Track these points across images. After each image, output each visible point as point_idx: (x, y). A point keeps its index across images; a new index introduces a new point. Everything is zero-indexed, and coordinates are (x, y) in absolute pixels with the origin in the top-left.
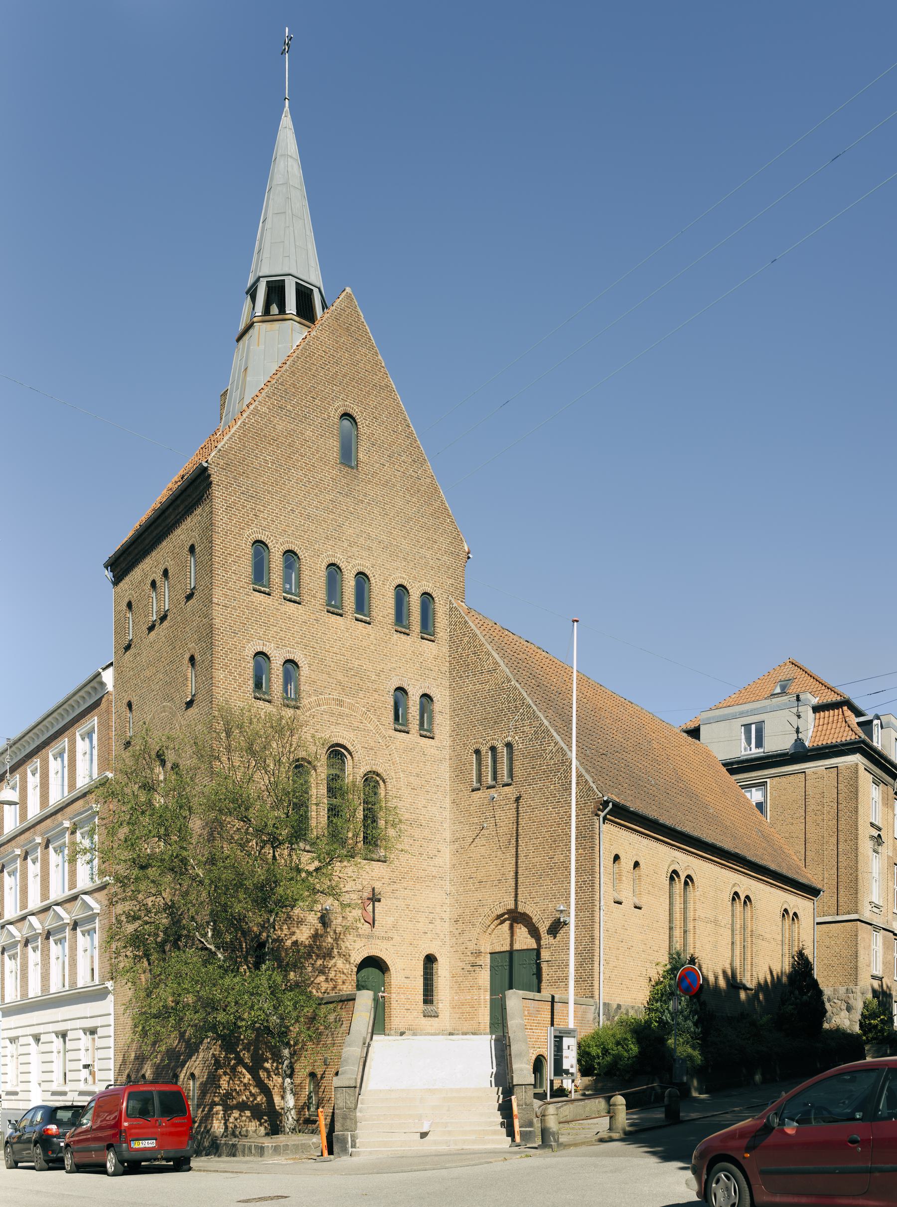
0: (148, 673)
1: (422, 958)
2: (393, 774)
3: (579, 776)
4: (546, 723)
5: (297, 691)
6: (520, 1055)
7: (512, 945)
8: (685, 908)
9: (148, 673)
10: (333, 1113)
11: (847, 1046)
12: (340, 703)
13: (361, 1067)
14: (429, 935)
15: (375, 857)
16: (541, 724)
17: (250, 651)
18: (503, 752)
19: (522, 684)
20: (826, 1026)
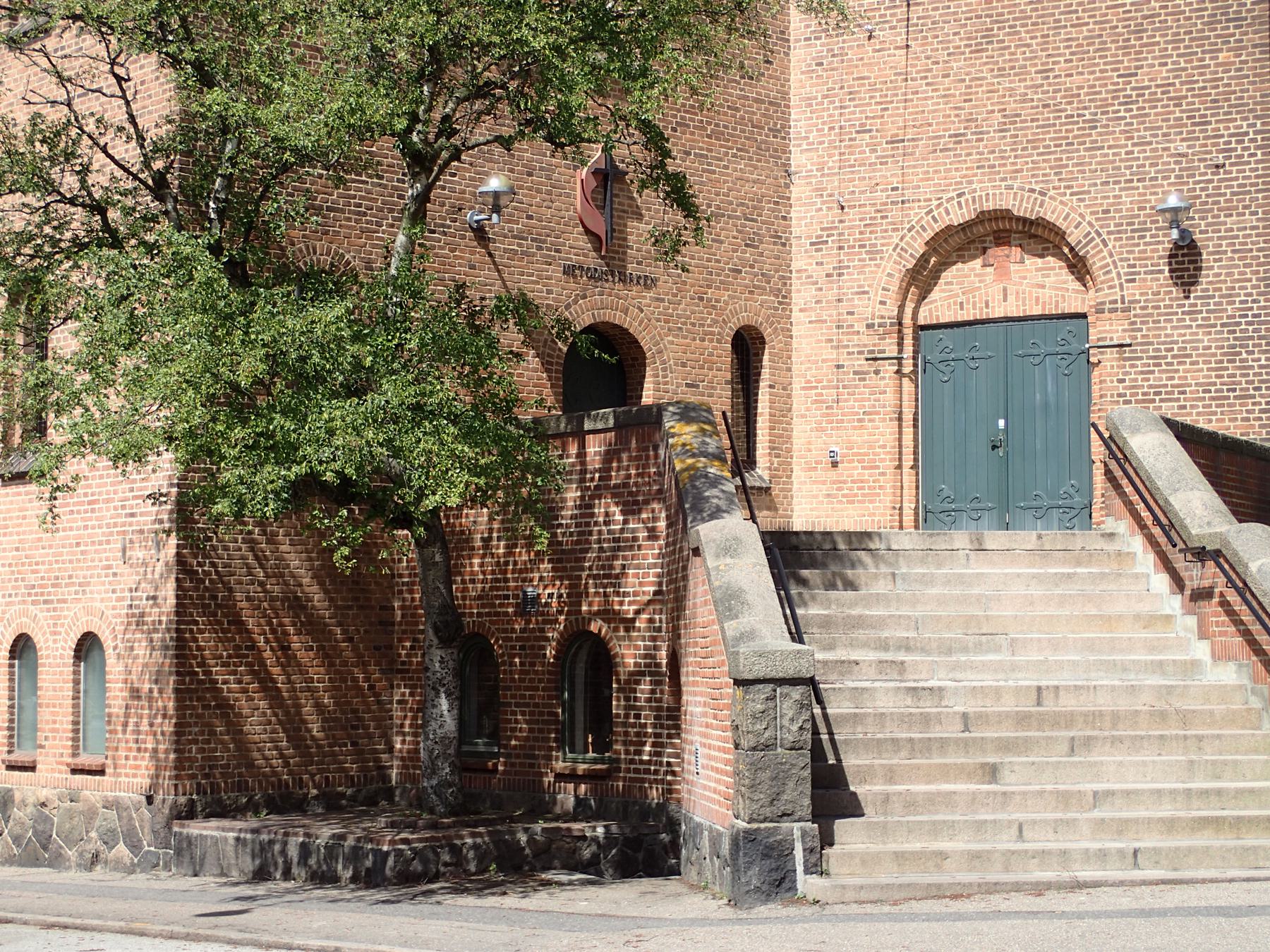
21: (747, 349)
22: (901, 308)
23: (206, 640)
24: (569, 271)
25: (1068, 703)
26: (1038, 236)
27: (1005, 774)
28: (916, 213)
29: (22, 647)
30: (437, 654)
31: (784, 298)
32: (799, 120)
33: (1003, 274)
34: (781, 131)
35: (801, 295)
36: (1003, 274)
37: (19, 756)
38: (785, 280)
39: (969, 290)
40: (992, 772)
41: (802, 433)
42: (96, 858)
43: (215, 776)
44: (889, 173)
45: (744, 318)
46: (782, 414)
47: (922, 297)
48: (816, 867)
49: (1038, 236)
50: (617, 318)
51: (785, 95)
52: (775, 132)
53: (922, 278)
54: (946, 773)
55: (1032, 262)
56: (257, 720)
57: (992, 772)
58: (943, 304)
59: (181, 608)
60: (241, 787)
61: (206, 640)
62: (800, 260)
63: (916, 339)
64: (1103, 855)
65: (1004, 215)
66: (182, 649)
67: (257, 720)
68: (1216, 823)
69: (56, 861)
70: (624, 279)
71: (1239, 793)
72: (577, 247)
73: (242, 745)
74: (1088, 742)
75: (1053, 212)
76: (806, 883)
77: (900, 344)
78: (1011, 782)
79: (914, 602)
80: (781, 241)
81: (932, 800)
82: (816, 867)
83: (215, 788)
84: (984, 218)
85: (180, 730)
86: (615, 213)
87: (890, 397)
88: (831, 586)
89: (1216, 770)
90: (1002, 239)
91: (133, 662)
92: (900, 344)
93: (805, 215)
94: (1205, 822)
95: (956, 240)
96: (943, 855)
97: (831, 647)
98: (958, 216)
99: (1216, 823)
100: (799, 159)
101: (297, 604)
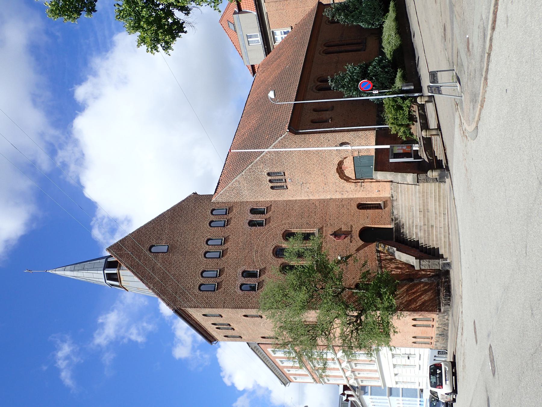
0: (250, 331)
1: (359, 210)
2: (283, 227)
3: (275, 147)
4: (258, 158)
5: (490, 358)
6: (403, 177)
7: (439, 187)
8: (347, 45)
9: (250, 331)
10: (507, 24)
11: (71, 96)
12: (257, 251)
13: (458, 243)
14: (349, 207)
15: (197, 314)
16: (259, 160)
17: (239, 291)
18: (404, 402)
19: (400, 101)
20: (146, 303)
21: (362, 206)
22: (353, 182)
23: (413, 306)
24: (351, 242)
25: (422, 207)
26: (340, 164)
27: (433, 224)
28: (337, 181)
29: (414, 326)
30: (415, 282)
31: (352, 199)
32: (322, 197)
33: (347, 168)
34: (324, 200)
35: (351, 196)
36: (347, 168)
37: (432, 320)
38: (349, 199)
39: (349, 171)
40: (432, 226)
41: (374, 196)
42: (447, 319)
43: (433, 306)
44: (331, 185)
45: (356, 207)
46: (370, 199)
47: (351, 179)
48: (446, 259)
49: (340, 164)
50: (358, 232)
51: (318, 200)
52: (324, 202)
53: (347, 179)
54: (432, 233)
55: (344, 164)
56: (425, 298)
57: (432, 226)
58: (352, 176)
59: (408, 311)
60: (436, 300)
61: (413, 306)
62: (345, 196)
63: (358, 179)
64: (444, 219)
65: (337, 169)
66: (415, 310)
67: (425, 298)
68: (439, 199)
69: (448, 323)
70: (351, 231)
71: (435, 192)
72: (347, 240)
73: (429, 300)
74: (427, 209)
75: (337, 163)
76: (448, 261)
77: (359, 182)
78: (434, 224)
79: (406, 217)
80: (342, 200)
81: (436, 237)
82: (446, 259)
83: (436, 305)
84: (338, 172)
85: (427, 311)
86: (378, 375)
87: (368, 184)
88: (403, 228)
89: (431, 193)
90: (341, 168)
91: (416, 316)
92: (359, 182)
93: (338, 196)
94: (439, 201)
95: (341, 175)
96: (444, 242)
97: (413, 234)
98: (337, 175)
99: (439, 199)
100: (329, 197)
101: (407, 290)
